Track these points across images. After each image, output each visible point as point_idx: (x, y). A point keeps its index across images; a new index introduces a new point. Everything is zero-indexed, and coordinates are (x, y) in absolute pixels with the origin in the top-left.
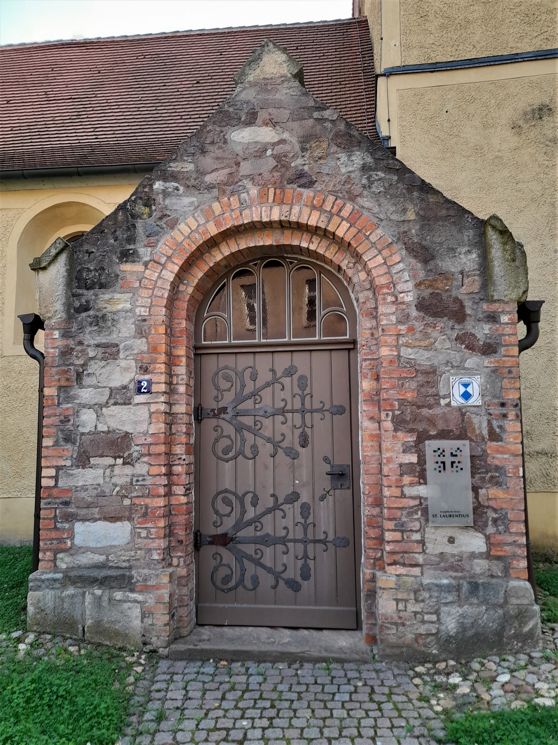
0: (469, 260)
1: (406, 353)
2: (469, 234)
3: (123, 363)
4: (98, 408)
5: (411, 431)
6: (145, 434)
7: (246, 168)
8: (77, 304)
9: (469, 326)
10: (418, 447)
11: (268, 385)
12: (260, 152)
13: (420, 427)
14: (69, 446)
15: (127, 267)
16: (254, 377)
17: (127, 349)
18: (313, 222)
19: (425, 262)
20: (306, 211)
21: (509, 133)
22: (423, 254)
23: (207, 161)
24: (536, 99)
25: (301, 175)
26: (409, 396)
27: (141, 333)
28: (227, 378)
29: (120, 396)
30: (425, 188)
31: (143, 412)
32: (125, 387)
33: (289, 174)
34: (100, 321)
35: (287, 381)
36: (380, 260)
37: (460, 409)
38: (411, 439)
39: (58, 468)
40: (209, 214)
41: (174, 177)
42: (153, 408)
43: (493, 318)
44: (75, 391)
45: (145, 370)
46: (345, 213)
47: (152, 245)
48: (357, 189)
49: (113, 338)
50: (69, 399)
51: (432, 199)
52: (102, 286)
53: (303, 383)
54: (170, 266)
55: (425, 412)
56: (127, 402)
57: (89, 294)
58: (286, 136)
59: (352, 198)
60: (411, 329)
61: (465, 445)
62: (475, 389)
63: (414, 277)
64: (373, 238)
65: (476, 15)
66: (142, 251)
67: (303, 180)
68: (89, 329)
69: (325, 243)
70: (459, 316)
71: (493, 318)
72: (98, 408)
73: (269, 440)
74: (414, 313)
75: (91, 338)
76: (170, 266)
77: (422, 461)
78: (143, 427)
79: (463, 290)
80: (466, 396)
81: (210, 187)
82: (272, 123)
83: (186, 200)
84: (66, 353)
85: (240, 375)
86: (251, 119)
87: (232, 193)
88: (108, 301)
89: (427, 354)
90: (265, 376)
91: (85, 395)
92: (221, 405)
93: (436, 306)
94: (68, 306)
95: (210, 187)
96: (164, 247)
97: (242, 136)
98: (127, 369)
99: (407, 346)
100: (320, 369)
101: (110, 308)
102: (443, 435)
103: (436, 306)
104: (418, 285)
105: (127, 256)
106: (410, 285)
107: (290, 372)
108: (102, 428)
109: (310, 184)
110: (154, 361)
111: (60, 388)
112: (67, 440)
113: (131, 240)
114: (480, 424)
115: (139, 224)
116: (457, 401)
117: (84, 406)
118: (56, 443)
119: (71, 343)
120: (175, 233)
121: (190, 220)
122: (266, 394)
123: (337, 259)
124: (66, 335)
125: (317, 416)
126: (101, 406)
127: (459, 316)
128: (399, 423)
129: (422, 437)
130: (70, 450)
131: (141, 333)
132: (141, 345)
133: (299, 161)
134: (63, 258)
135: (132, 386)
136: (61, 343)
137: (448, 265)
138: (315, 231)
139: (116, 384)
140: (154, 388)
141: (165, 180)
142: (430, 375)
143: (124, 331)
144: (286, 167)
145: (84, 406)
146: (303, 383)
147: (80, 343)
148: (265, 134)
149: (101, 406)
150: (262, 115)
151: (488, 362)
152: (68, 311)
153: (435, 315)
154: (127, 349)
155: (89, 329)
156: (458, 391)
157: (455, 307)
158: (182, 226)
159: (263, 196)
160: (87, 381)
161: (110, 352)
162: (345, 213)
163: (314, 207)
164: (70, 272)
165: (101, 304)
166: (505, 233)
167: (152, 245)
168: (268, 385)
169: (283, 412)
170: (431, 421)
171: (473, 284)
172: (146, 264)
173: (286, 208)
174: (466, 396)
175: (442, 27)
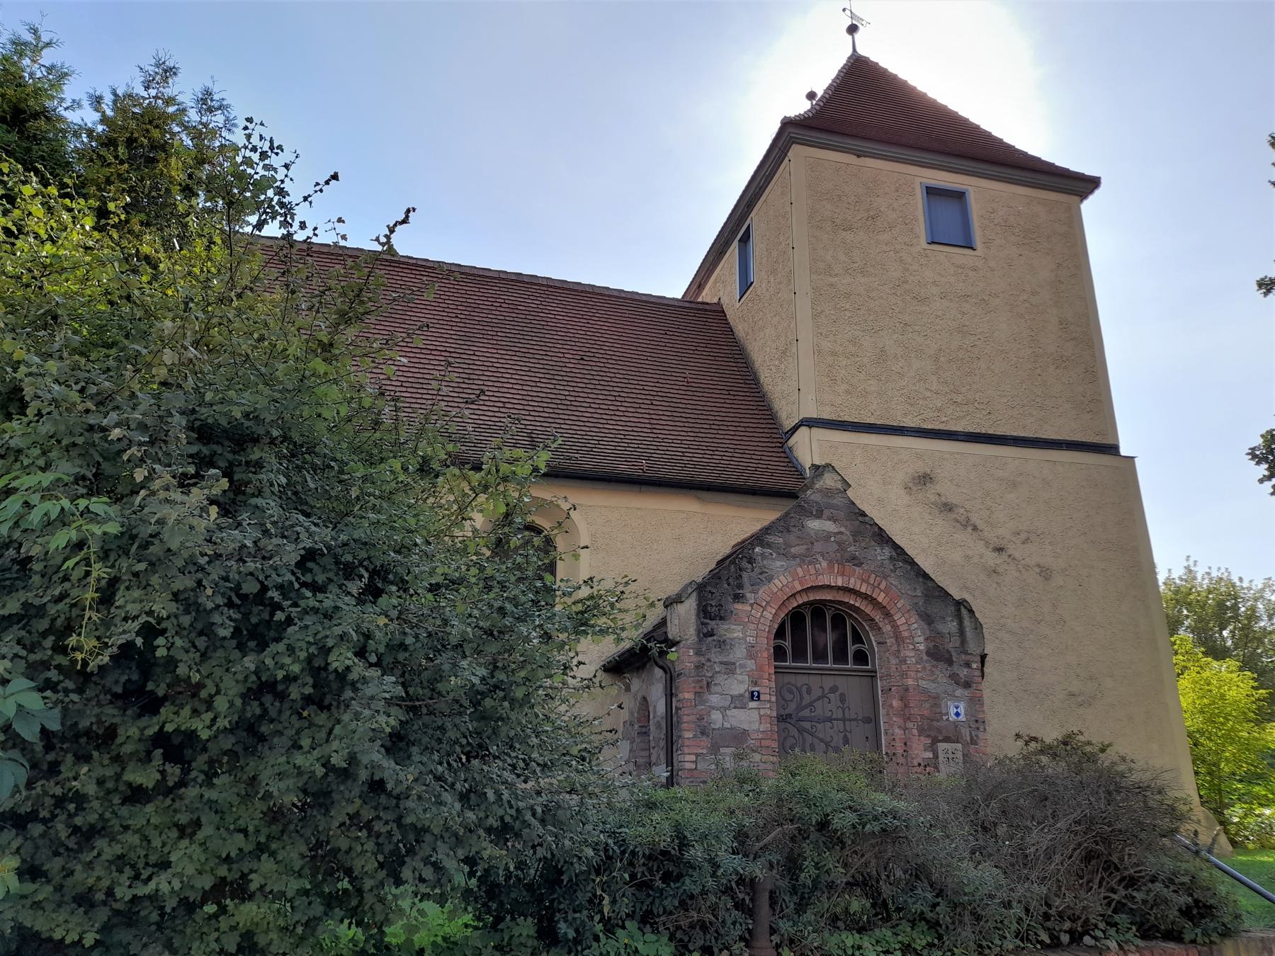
0: (952, 626)
1: (922, 683)
2: (951, 609)
3: (740, 677)
4: (724, 710)
5: (928, 736)
6: (758, 731)
7: (818, 547)
8: (705, 631)
9: (955, 668)
10: (933, 747)
11: (819, 699)
12: (827, 537)
13: (933, 733)
14: (704, 738)
15: (739, 606)
16: (809, 692)
17: (742, 666)
18: (863, 590)
19: (929, 624)
20: (859, 582)
21: (902, 492)
22: (928, 619)
23: (792, 538)
24: (921, 468)
25: (854, 558)
26: (926, 713)
27: (750, 656)
28: (791, 692)
29: (738, 702)
30: (926, 576)
31: (755, 715)
32: (742, 695)
33: (847, 556)
34: (721, 644)
35: (831, 696)
36: (903, 620)
37: (954, 722)
38: (929, 741)
39: (697, 755)
40: (795, 576)
41: (769, 545)
42: (762, 712)
43: (968, 665)
44: (707, 696)
45: (756, 684)
46: (883, 586)
47: (755, 592)
48: (887, 572)
49: (731, 658)
50: (703, 702)
51: (930, 584)
52: (722, 618)
53: (843, 698)
54: (769, 609)
55: (935, 723)
56: (744, 707)
57: (713, 623)
58: (843, 529)
59: (885, 577)
60: (924, 668)
61: (959, 746)
62: (962, 710)
63: (923, 633)
64: (899, 605)
65: (873, 388)
66: (748, 595)
67: (856, 561)
68: (714, 650)
69: (865, 602)
70: (950, 662)
71: (968, 665)
72: (724, 710)
73: (822, 740)
74: (925, 657)
75: (716, 657)
76: (769, 609)
77: (936, 757)
78: (755, 726)
79: (951, 645)
80: (957, 714)
81: (794, 557)
82: (833, 519)
83: (778, 563)
84: (699, 667)
85: (799, 690)
86: (819, 515)
87: (810, 563)
88: (726, 630)
89: (934, 685)
90: (816, 693)
91: (714, 699)
92: (787, 712)
93: (938, 655)
94: (698, 631)
95: (794, 557)
96: (763, 593)
97: (814, 525)
98: (742, 682)
99: (923, 679)
100: (852, 687)
101: (728, 635)
102: (947, 740)
103: (938, 655)
104: (926, 639)
105: (738, 598)
106: (921, 639)
107: (834, 689)
108: (727, 725)
109: (860, 565)
110: (761, 677)
111: (696, 693)
112: (703, 733)
113: (740, 586)
114: (966, 733)
115: (745, 575)
116: (953, 717)
117: (713, 708)
118: (695, 736)
119: (703, 660)
120: (772, 586)
121: (782, 578)
122: (818, 704)
123: (873, 614)
124: (698, 653)
125: (854, 723)
126: (726, 709)
127: (950, 662)
128: (921, 731)
129: (935, 741)
130: (706, 741)
131: (750, 656)
132: (751, 664)
133: (853, 548)
134: (695, 594)
135: (747, 695)
136: (695, 659)
137: (941, 627)
138: (865, 597)
139: (736, 693)
140: (762, 697)
141: (763, 546)
142: (935, 700)
143: (739, 653)
144: (844, 550)
145: (713, 708)
146: (843, 698)
147: (709, 660)
148: (829, 526)
149: (726, 709)
150: (826, 513)
151: (966, 693)
152: (698, 636)
153: (937, 660)
154: (742, 666)
155: (714, 650)
156: (953, 711)
157: (947, 655)
158: (776, 581)
159: (831, 566)
160: (714, 689)
161: (730, 668)
162: (883, 586)
163: (863, 580)
164: (698, 605)
165: (723, 632)
166: (971, 611)
167: (755, 592)
168: (819, 699)
169: (830, 720)
170: (939, 730)
171: (956, 642)
172: (752, 605)
173: (846, 579)
174: (957, 714)
175: (847, 392)
